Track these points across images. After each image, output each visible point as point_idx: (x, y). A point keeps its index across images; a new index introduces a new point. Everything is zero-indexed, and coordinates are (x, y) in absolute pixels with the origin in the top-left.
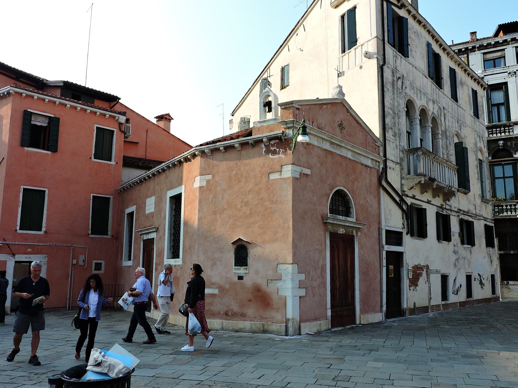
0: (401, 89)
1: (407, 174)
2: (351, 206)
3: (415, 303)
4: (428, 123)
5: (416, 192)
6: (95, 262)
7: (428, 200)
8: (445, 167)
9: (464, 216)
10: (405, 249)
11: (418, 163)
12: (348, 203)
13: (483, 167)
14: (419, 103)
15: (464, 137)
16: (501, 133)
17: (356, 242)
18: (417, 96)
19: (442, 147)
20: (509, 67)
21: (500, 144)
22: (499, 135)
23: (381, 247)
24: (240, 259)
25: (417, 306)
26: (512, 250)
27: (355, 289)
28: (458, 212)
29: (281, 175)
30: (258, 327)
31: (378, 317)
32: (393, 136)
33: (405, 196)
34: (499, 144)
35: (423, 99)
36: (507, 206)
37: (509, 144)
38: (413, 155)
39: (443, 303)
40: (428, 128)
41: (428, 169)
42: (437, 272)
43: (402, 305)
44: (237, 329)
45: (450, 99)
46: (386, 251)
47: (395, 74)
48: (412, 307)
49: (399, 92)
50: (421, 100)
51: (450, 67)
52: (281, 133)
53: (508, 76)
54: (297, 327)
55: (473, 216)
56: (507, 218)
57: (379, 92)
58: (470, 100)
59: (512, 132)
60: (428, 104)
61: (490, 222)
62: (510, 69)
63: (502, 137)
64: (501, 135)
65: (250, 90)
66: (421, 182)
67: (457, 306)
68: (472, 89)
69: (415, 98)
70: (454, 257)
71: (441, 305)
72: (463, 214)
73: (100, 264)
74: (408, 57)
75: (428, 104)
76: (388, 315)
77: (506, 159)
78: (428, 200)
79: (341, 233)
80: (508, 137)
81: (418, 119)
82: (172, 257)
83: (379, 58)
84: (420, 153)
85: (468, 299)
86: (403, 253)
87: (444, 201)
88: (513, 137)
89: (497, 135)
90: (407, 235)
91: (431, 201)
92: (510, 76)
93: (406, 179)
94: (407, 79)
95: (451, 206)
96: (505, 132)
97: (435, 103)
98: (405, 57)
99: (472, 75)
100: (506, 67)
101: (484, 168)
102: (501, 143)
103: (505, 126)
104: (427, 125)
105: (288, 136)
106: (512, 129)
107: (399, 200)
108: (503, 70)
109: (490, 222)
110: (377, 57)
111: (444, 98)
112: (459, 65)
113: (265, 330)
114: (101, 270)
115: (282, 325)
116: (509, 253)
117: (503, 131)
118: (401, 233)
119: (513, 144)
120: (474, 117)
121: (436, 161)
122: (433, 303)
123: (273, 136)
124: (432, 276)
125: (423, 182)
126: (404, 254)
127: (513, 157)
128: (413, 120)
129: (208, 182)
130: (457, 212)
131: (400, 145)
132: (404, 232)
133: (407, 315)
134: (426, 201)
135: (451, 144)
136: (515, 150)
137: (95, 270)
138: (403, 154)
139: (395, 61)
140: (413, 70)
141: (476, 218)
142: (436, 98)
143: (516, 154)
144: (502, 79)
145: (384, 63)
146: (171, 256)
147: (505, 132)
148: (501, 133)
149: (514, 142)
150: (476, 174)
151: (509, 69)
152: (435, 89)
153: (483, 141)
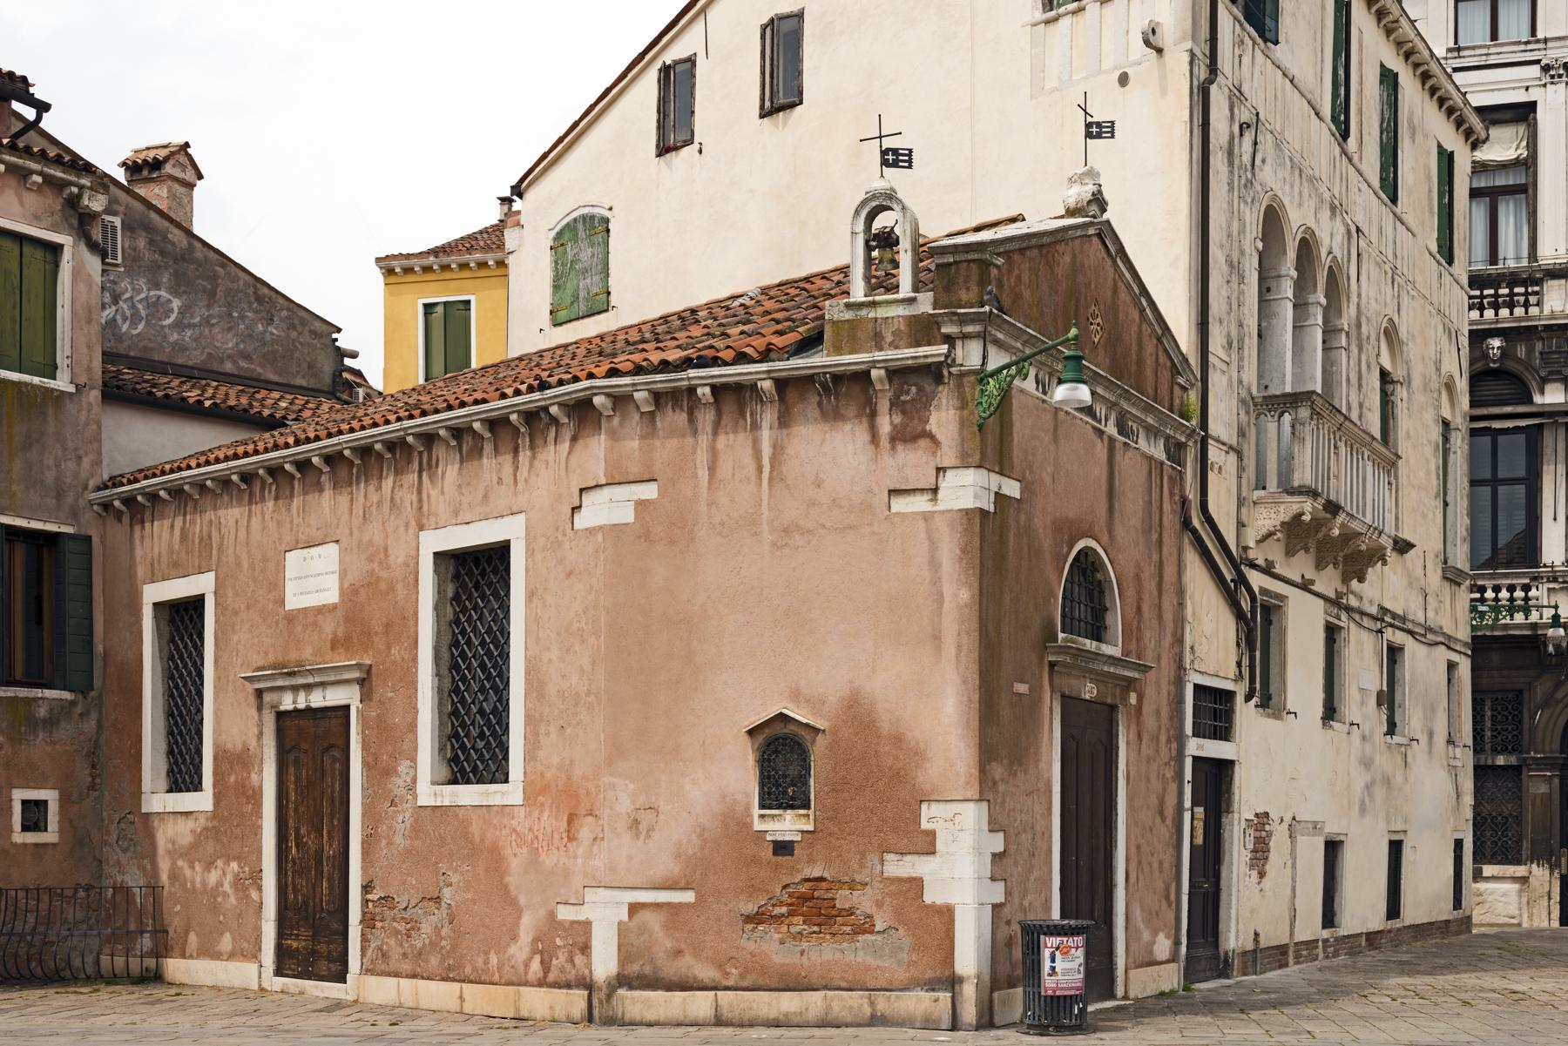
0: (1249, 167)
1: (1254, 486)
2: (1108, 605)
3: (1256, 935)
4: (1315, 291)
5: (1275, 552)
6: (19, 795)
7: (1303, 576)
8: (1366, 457)
9: (1394, 633)
10: (1238, 752)
11: (1296, 450)
12: (1102, 592)
13: (1452, 450)
14: (1297, 218)
15: (1408, 339)
16: (1496, 307)
17: (1120, 728)
18: (1292, 194)
19: (1348, 380)
20: (1546, 41)
21: (1491, 352)
22: (1489, 314)
23: (1180, 740)
24: (781, 785)
25: (1264, 943)
26: (1500, 753)
27: (1116, 885)
28: (1378, 620)
29: (934, 500)
30: (851, 1008)
31: (1170, 978)
32: (1223, 347)
33: (1246, 565)
34: (1488, 348)
35: (1306, 204)
36: (1497, 589)
37: (1521, 351)
38: (1280, 417)
39: (1326, 934)
40: (1312, 309)
41: (1323, 470)
42: (1316, 826)
43: (1222, 938)
44: (772, 1016)
45: (1375, 193)
46: (1195, 758)
47: (1236, 111)
48: (1250, 946)
49: (1243, 181)
50: (1300, 205)
51: (1382, 66)
52: (939, 355)
53: (1540, 79)
54: (986, 1003)
55: (1417, 633)
56: (1496, 633)
57: (1194, 185)
58: (1430, 191)
59: (1537, 305)
60: (1317, 221)
61: (1460, 652)
62: (1548, 52)
63: (1502, 322)
64: (1496, 314)
65: (607, 98)
66: (1304, 518)
67: (1360, 945)
68: (1440, 146)
69: (1286, 201)
70: (1359, 780)
71: (1320, 943)
72: (1392, 625)
73: (41, 805)
74: (1276, 43)
75: (1317, 221)
76: (1192, 973)
77: (1509, 409)
78: (1303, 576)
79: (1087, 697)
80: (1523, 324)
81: (1292, 278)
82: (449, 777)
83: (1197, 52)
84: (1304, 413)
85: (1389, 922)
86: (1232, 763)
87: (1346, 579)
88: (1536, 327)
89: (1482, 316)
90: (1246, 702)
91: (1312, 582)
92: (1549, 80)
93: (1252, 504)
94: (1267, 125)
95: (1361, 598)
96: (1511, 306)
97: (1338, 213)
98: (1266, 41)
99: (1447, 91)
100: (1538, 41)
101: (1455, 453)
102: (1493, 348)
103: (1513, 279)
104: (1310, 301)
105: (962, 365)
106: (1536, 293)
107: (1232, 581)
108: (1524, 54)
109: (1460, 652)
110: (1191, 50)
111: (1360, 190)
112: (1407, 56)
113: (879, 1014)
114: (46, 830)
115: (941, 998)
116: (1490, 762)
117: (1504, 301)
118: (1228, 696)
119: (1537, 354)
120: (1438, 256)
121: (1344, 439)
122: (1302, 935)
123: (910, 362)
124: (1302, 840)
125: (1307, 518)
126: (1237, 767)
127: (1530, 401)
128: (1273, 284)
129: (641, 505)
130: (1375, 619)
131: (1240, 382)
132: (1241, 690)
133: (1235, 973)
134: (1298, 580)
135: (1372, 367)
136: (1541, 378)
137: (25, 828)
138: (1247, 413)
139: (1237, 60)
140: (1283, 89)
141: (1424, 640)
142: (1340, 193)
143: (1542, 392)
144: (1519, 88)
145: (1210, 73)
146: (445, 772)
147: (1511, 306)
148: (1496, 307)
149: (1539, 346)
150: (1434, 477)
151: (1545, 49)
152: (1338, 158)
153: (1459, 350)
